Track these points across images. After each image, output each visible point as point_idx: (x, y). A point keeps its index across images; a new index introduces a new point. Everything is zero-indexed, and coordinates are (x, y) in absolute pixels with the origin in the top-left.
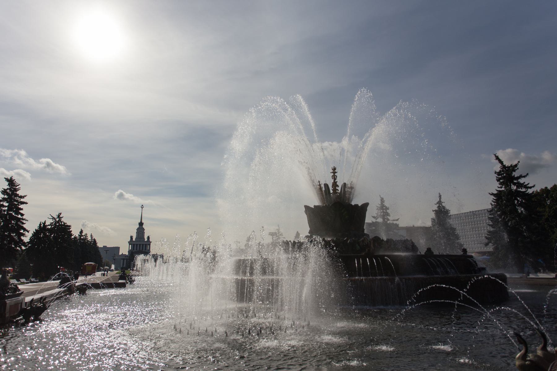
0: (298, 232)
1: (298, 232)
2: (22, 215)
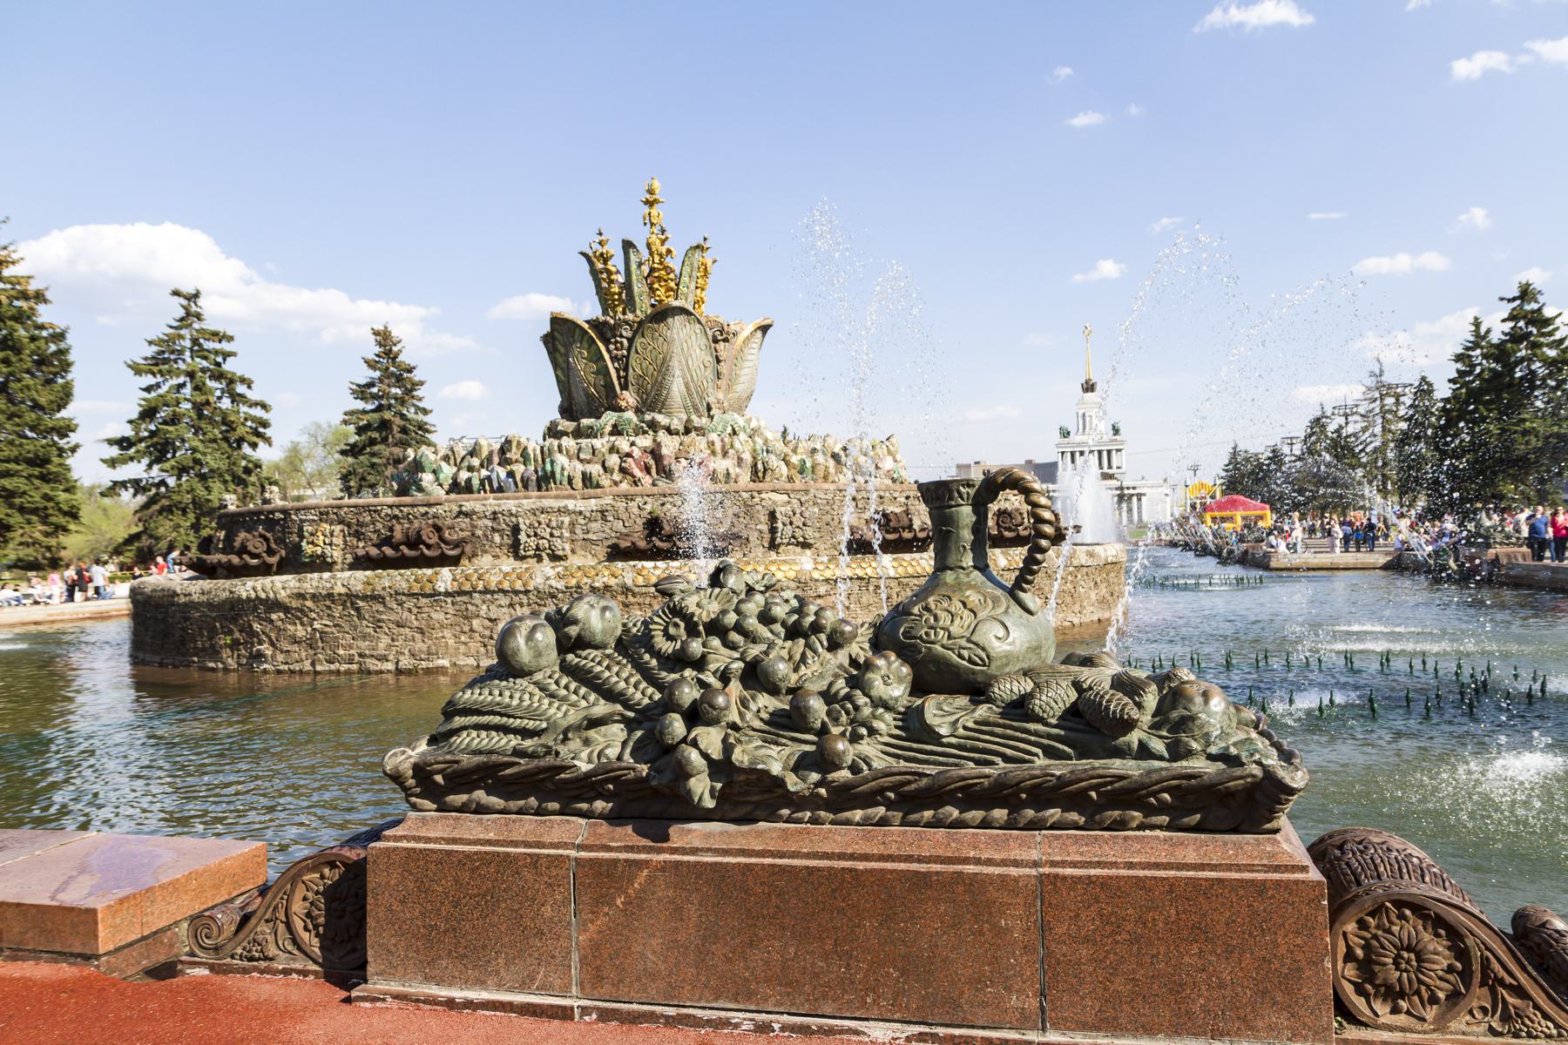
2: (425, 412)
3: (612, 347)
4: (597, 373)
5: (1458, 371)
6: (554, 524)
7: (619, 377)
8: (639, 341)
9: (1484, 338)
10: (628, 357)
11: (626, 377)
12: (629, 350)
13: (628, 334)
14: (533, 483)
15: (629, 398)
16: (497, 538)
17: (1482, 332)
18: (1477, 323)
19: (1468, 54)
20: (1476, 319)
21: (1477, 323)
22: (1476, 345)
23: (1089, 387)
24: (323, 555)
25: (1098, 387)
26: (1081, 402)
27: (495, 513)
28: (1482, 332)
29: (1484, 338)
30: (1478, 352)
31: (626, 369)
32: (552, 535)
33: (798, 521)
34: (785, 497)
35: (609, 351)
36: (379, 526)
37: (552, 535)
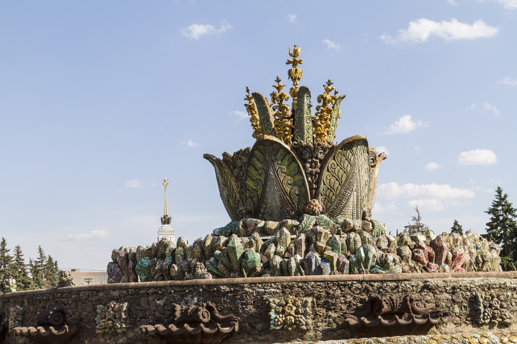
0: (456, 223)
1: (456, 223)
3: (308, 165)
4: (294, 184)
5: (492, 219)
6: (502, 297)
7: (311, 189)
8: (331, 162)
9: (503, 199)
10: (320, 174)
11: (317, 189)
12: (322, 168)
13: (321, 156)
14: (347, 267)
15: (318, 204)
16: (457, 310)
17: (503, 196)
18: (499, 191)
19: (480, 41)
20: (499, 188)
21: (499, 191)
22: (498, 204)
23: (166, 220)
24: (297, 324)
25: (172, 221)
26: (160, 231)
27: (454, 288)
28: (503, 196)
29: (503, 199)
30: (500, 208)
31: (318, 183)
32: (502, 307)
33: (496, 303)
34: (395, 284)
35: (305, 168)
36: (349, 298)
37: (502, 307)
